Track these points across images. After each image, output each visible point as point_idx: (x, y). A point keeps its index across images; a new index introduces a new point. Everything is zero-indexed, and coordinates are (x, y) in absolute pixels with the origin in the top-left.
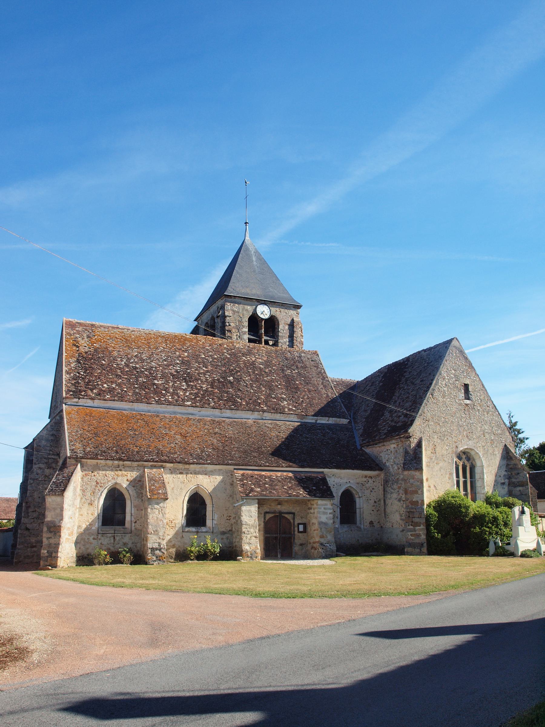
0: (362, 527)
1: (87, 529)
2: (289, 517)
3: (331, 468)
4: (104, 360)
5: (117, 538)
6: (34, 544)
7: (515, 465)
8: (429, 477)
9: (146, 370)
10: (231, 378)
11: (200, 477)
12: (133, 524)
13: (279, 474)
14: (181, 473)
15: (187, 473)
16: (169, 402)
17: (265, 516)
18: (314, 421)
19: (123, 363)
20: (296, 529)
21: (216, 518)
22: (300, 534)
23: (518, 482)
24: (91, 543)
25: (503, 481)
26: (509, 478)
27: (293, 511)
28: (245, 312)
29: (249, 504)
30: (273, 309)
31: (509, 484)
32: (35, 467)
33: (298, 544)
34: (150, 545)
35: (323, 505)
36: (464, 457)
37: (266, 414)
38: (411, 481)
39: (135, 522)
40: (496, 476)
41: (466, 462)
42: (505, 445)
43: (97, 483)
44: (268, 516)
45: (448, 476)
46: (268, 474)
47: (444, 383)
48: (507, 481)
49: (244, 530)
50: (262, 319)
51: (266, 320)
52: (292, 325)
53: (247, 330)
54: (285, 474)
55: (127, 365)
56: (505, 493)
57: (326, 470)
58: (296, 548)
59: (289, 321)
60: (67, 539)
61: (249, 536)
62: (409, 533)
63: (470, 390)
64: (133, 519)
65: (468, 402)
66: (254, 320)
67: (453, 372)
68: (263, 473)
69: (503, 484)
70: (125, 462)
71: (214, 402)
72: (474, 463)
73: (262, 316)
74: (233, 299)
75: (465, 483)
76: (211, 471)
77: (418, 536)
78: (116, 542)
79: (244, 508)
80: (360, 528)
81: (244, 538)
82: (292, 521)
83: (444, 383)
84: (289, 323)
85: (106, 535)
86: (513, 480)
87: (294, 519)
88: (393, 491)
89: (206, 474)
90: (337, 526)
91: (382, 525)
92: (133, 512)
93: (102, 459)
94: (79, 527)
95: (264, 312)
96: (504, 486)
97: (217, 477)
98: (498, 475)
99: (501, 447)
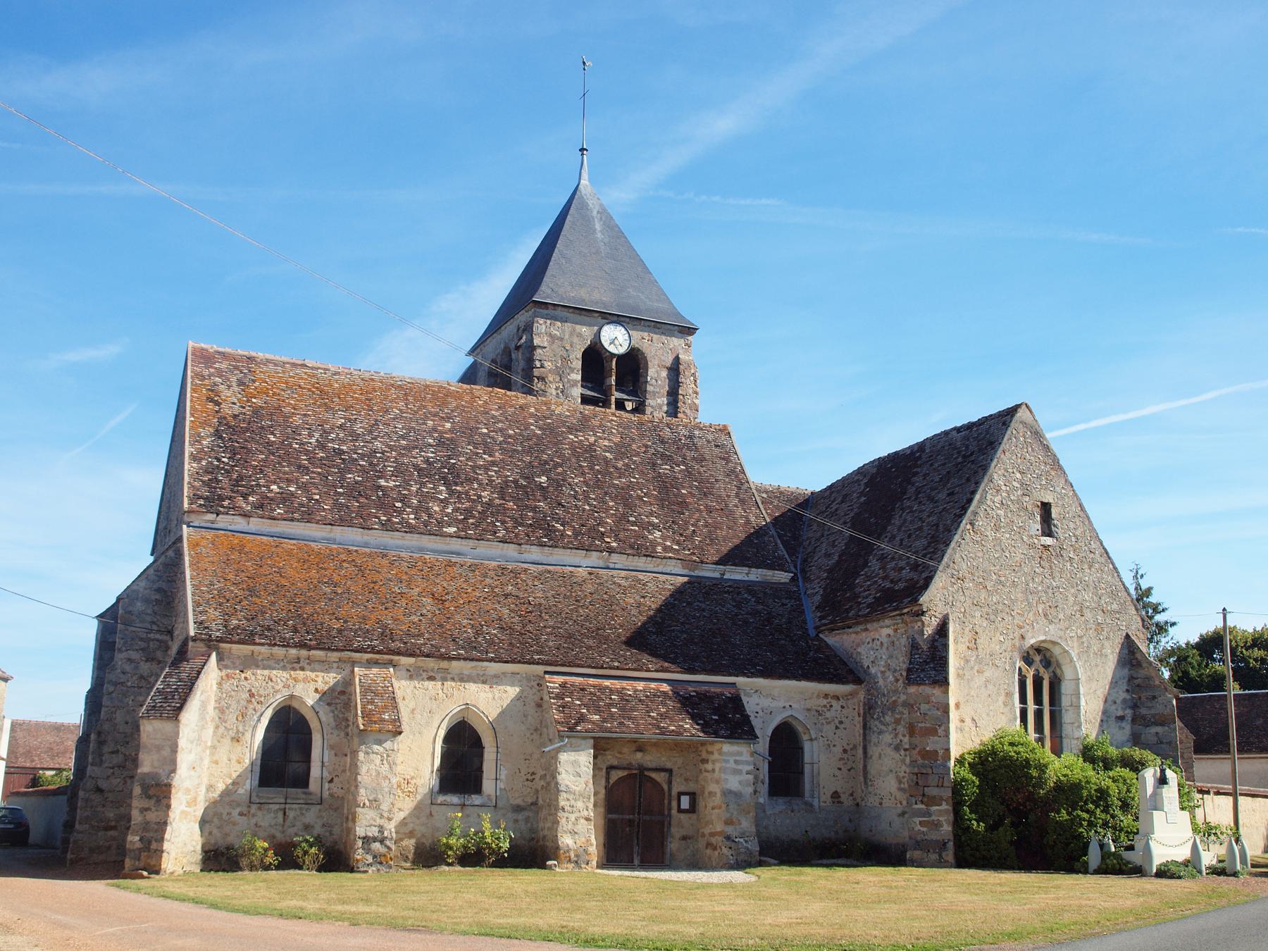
0: (816, 803)
1: (226, 793)
2: (660, 777)
3: (753, 675)
4: (272, 433)
5: (291, 814)
6: (113, 824)
7: (1148, 678)
8: (962, 700)
9: (362, 456)
10: (544, 479)
11: (472, 687)
12: (326, 786)
13: (640, 686)
14: (431, 678)
15: (444, 679)
16: (409, 525)
17: (608, 773)
18: (717, 575)
19: (313, 440)
20: (674, 804)
21: (503, 777)
22: (682, 816)
23: (1154, 716)
24: (234, 824)
25: (1120, 713)
26: (1135, 706)
27: (669, 765)
28: (576, 340)
29: (576, 749)
30: (636, 335)
31: (1133, 720)
32: (119, 657)
33: (678, 836)
34: (360, 831)
35: (732, 754)
36: (1037, 658)
37: (615, 557)
38: (924, 707)
39: (331, 781)
40: (1106, 701)
41: (1042, 670)
42: (1127, 636)
43: (252, 695)
44: (616, 775)
45: (1002, 698)
46: (617, 684)
47: (998, 499)
48: (1129, 712)
49: (562, 803)
50: (613, 355)
51: (620, 358)
52: (675, 370)
53: (579, 377)
54: (653, 685)
55: (322, 446)
56: (1125, 738)
57: (740, 681)
58: (673, 845)
59: (669, 360)
60: (183, 812)
61: (572, 817)
62: (917, 820)
63: (1053, 516)
64: (326, 774)
65: (1048, 541)
66: (594, 358)
67: (1018, 476)
68: (607, 683)
69: (1121, 718)
70: (313, 652)
71: (506, 529)
72: (1058, 671)
73: (612, 349)
74: (550, 311)
75: (1039, 715)
76: (496, 676)
77: (937, 825)
78: (288, 823)
79: (564, 757)
80: (812, 806)
81: (563, 821)
82: (665, 787)
83: (998, 499)
84: (669, 365)
85: (266, 806)
86: (1144, 711)
87: (670, 782)
88: (883, 727)
89: (484, 682)
90: (761, 800)
91: (859, 800)
92: (326, 759)
93: (262, 644)
94: (210, 787)
95: (616, 339)
96: (1124, 724)
97: (508, 688)
98: (1110, 699)
99: (1118, 640)
